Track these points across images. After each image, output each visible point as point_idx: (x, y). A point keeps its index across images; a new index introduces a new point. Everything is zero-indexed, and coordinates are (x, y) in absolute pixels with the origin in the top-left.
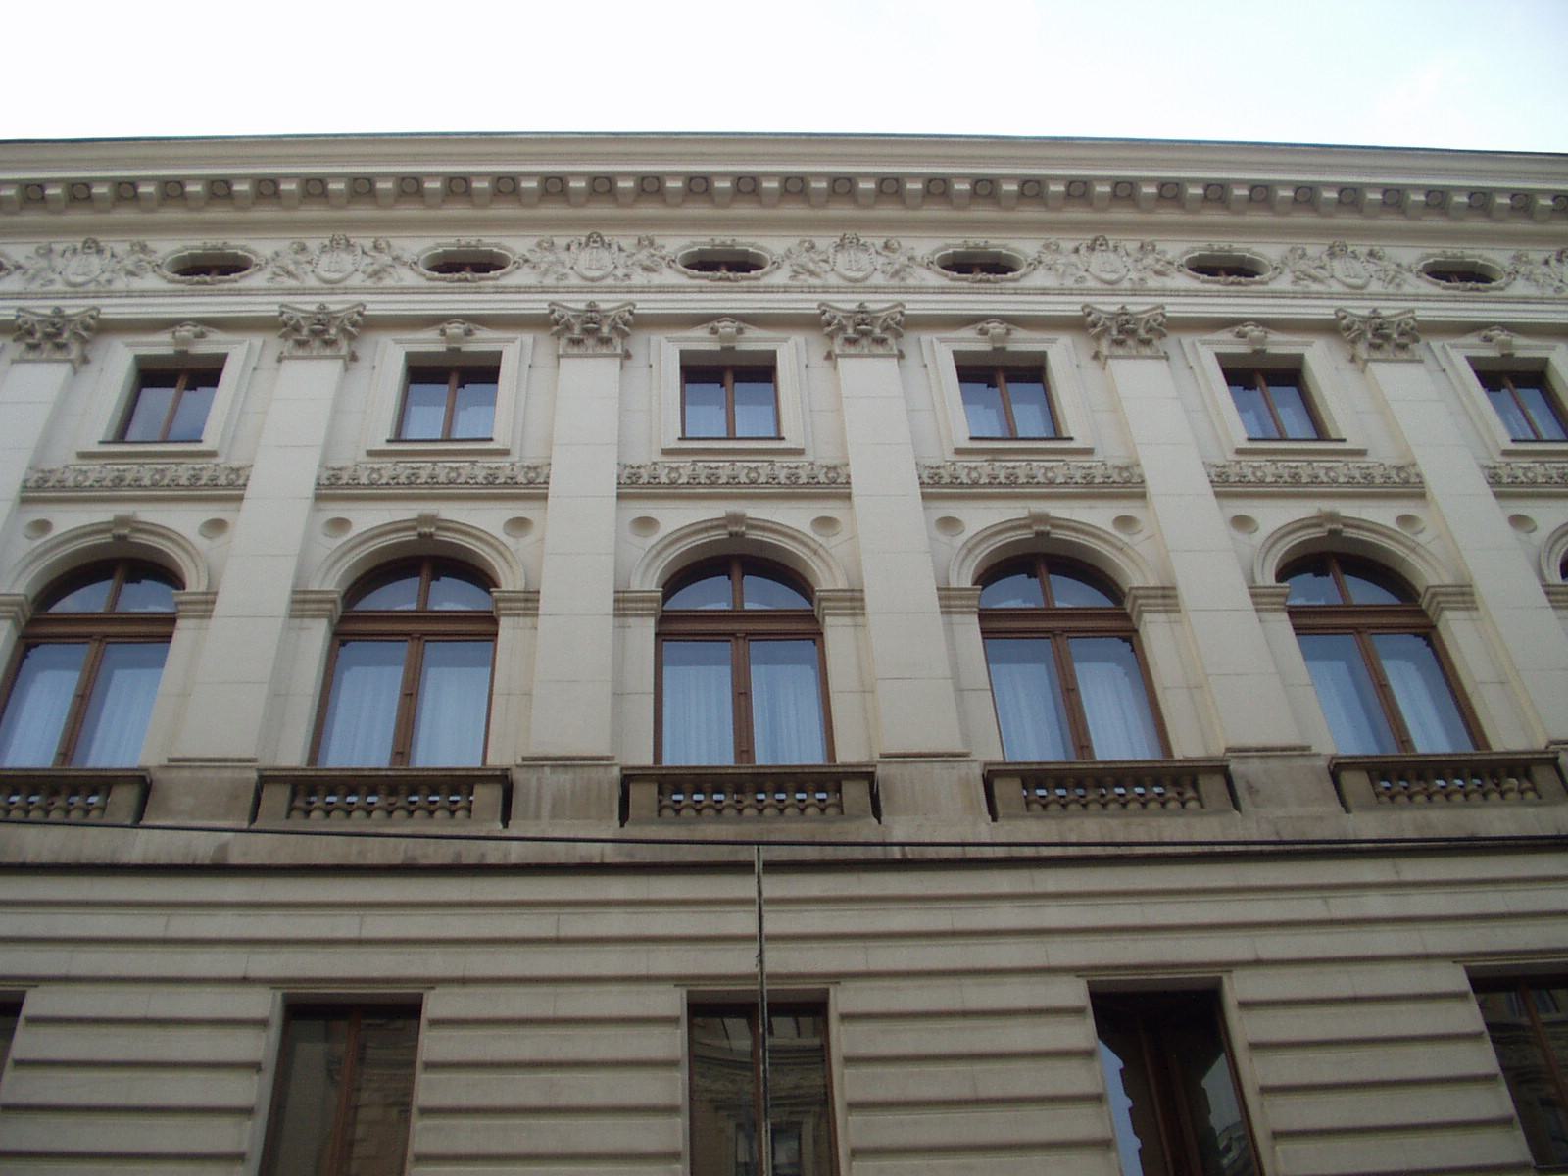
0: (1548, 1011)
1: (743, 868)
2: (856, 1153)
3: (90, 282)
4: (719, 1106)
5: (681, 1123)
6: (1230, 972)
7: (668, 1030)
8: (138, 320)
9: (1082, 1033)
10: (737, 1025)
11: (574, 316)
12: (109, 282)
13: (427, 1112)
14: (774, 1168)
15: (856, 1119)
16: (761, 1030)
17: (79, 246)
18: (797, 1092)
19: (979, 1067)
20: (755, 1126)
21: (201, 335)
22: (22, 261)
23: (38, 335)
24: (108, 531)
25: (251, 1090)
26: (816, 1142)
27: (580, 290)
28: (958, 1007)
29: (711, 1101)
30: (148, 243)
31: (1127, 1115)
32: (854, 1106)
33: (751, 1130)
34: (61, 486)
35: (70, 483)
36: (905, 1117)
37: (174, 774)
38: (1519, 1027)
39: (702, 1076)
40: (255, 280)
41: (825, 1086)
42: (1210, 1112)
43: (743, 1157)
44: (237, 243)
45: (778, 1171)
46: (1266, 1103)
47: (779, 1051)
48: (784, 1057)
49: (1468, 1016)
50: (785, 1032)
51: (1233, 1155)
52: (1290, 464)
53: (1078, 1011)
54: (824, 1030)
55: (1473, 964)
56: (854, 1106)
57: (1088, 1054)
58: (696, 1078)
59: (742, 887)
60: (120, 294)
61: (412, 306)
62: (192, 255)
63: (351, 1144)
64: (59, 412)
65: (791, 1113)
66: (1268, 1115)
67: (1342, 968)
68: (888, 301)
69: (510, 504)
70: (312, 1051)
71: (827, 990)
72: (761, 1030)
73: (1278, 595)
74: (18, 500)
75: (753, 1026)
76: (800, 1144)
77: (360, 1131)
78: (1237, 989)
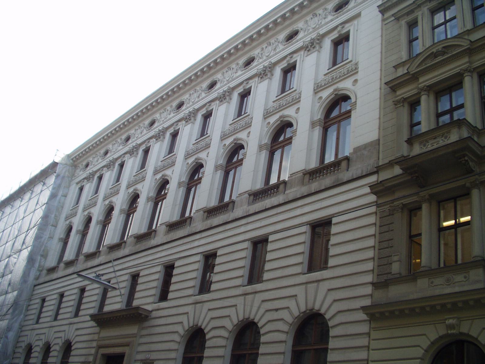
1: (110, 262)
3: (316, 26)
8: (278, 60)
11: (309, 43)
12: (321, 23)
17: (312, 16)
21: (343, 27)
22: (302, 27)
23: (309, 47)
24: (333, 94)
27: (313, 32)
30: (326, 7)
34: (321, 86)
35: (323, 85)
37: (293, 177)
40: (300, 35)
44: (295, 27)
52: (240, 123)
59: (110, 265)
60: (273, 55)
61: (247, 76)
62: (288, 35)
64: (317, 65)
68: (315, 34)
69: (351, 78)
73: (265, 146)
74: (264, 119)
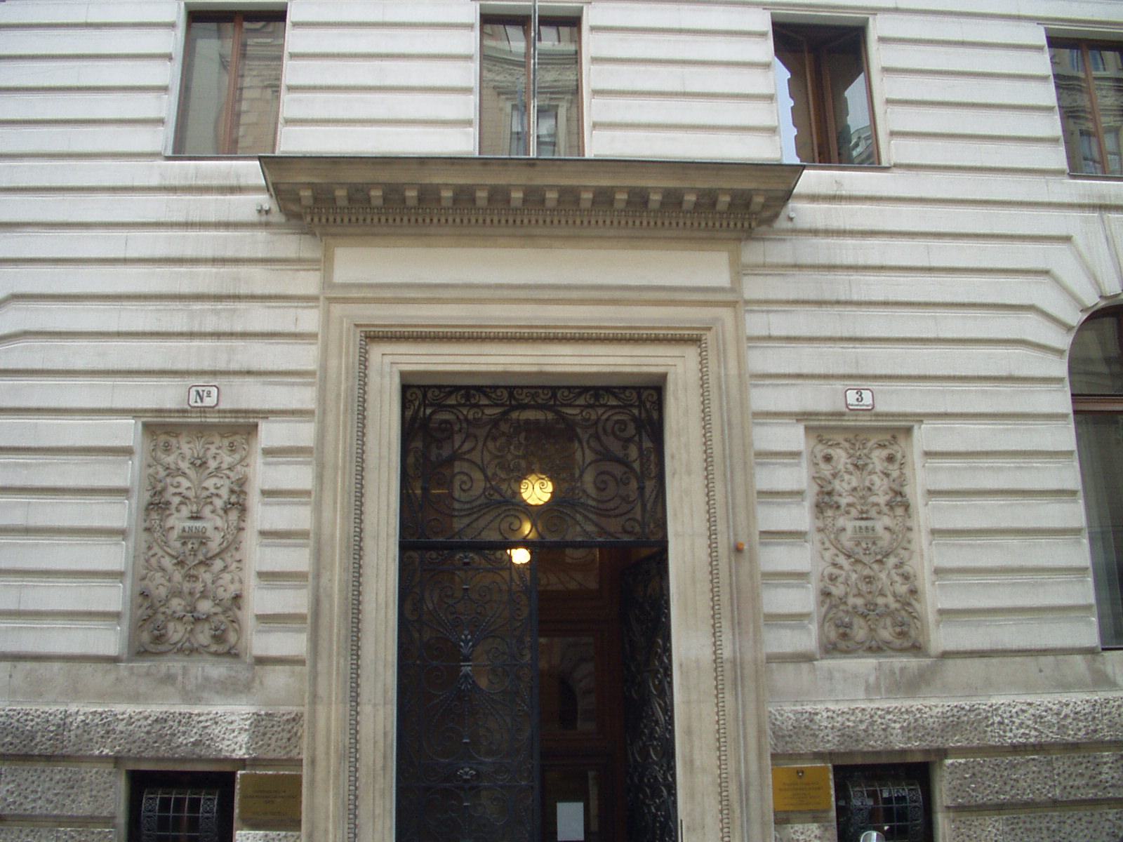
0: (1097, 69)
2: (595, 125)
4: (500, 92)
5: (474, 99)
6: (876, 14)
7: (465, 32)
9: (765, 50)
10: (514, 32)
13: (291, 89)
14: (538, 137)
15: (598, 101)
16: (533, 34)
18: (555, 84)
19: (688, 70)
20: (526, 107)
25: (168, 74)
26: (568, 120)
28: (676, 26)
29: (494, 88)
31: (790, 111)
32: (597, 93)
33: (523, 109)
36: (635, 102)
38: (1077, 79)
39: (490, 71)
41: (577, 80)
42: (847, 115)
43: (517, 128)
45: (541, 139)
46: (889, 110)
47: (544, 54)
48: (549, 59)
49: (1042, 64)
50: (550, 41)
51: (859, 150)
53: (763, 35)
54: (577, 39)
55: (1050, 26)
56: (597, 93)
57: (767, 66)
58: (485, 73)
63: (239, 115)
65: (551, 99)
66: (889, 120)
67: (955, 19)
70: (211, 46)
71: (582, 8)
72: (533, 34)
75: (526, 33)
76: (556, 123)
77: (244, 106)
78: (877, 29)
